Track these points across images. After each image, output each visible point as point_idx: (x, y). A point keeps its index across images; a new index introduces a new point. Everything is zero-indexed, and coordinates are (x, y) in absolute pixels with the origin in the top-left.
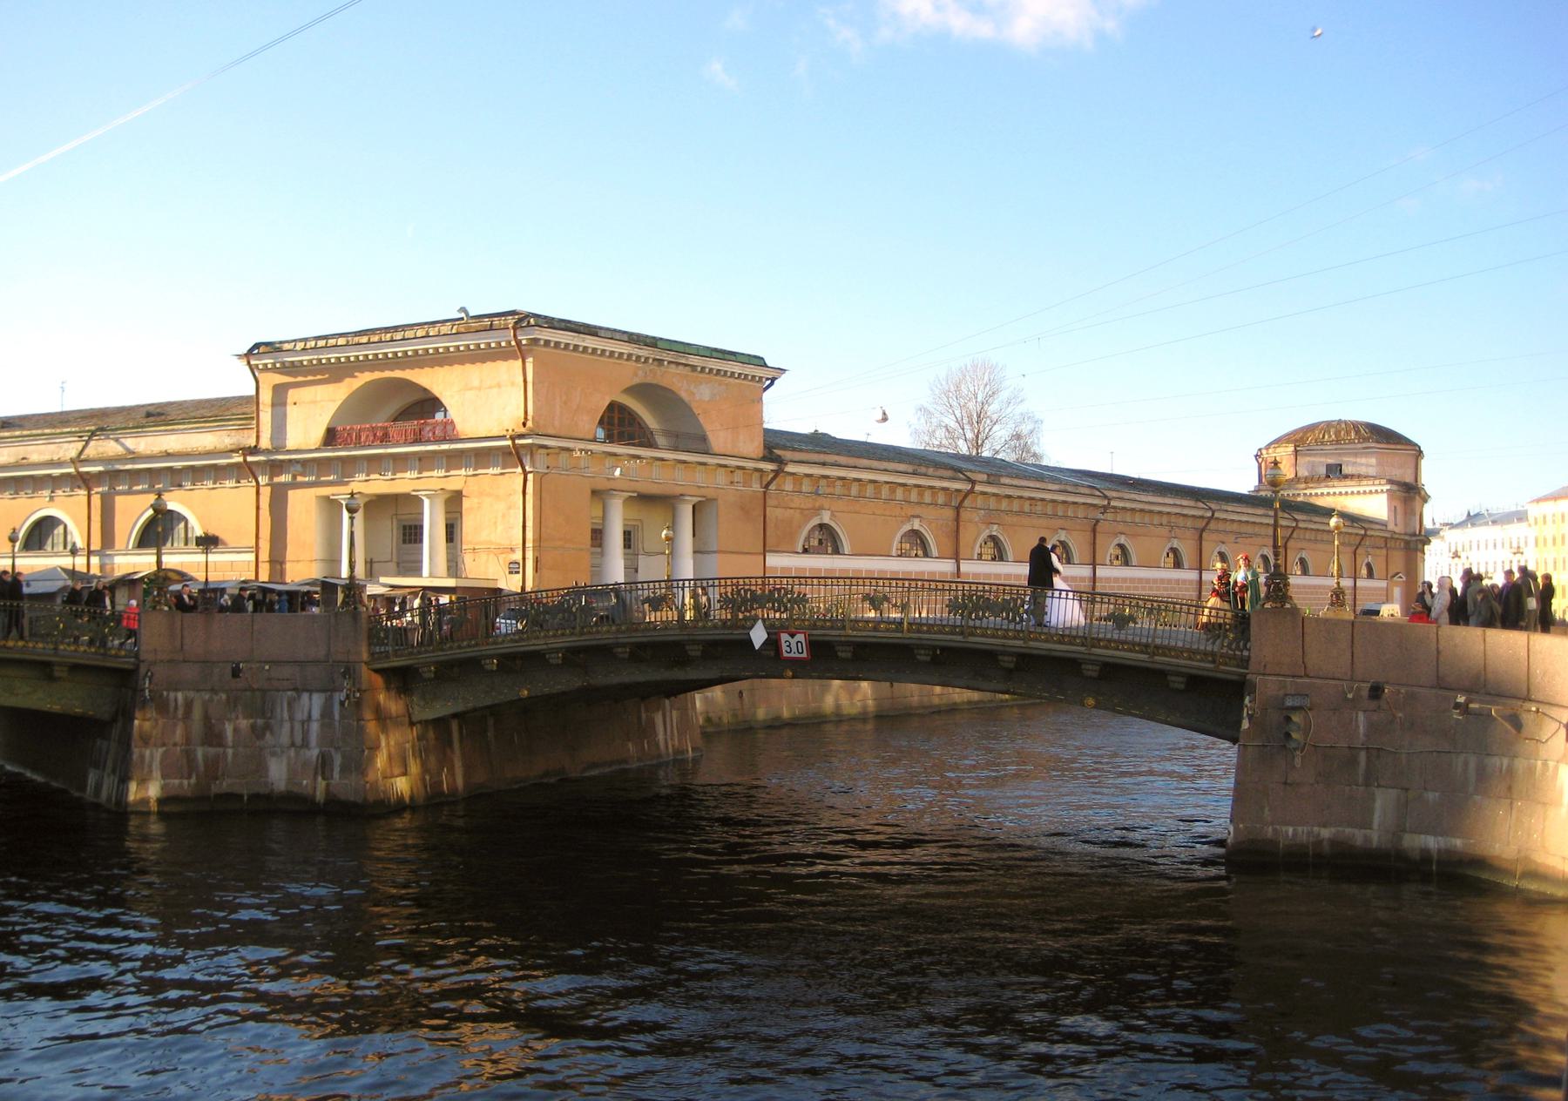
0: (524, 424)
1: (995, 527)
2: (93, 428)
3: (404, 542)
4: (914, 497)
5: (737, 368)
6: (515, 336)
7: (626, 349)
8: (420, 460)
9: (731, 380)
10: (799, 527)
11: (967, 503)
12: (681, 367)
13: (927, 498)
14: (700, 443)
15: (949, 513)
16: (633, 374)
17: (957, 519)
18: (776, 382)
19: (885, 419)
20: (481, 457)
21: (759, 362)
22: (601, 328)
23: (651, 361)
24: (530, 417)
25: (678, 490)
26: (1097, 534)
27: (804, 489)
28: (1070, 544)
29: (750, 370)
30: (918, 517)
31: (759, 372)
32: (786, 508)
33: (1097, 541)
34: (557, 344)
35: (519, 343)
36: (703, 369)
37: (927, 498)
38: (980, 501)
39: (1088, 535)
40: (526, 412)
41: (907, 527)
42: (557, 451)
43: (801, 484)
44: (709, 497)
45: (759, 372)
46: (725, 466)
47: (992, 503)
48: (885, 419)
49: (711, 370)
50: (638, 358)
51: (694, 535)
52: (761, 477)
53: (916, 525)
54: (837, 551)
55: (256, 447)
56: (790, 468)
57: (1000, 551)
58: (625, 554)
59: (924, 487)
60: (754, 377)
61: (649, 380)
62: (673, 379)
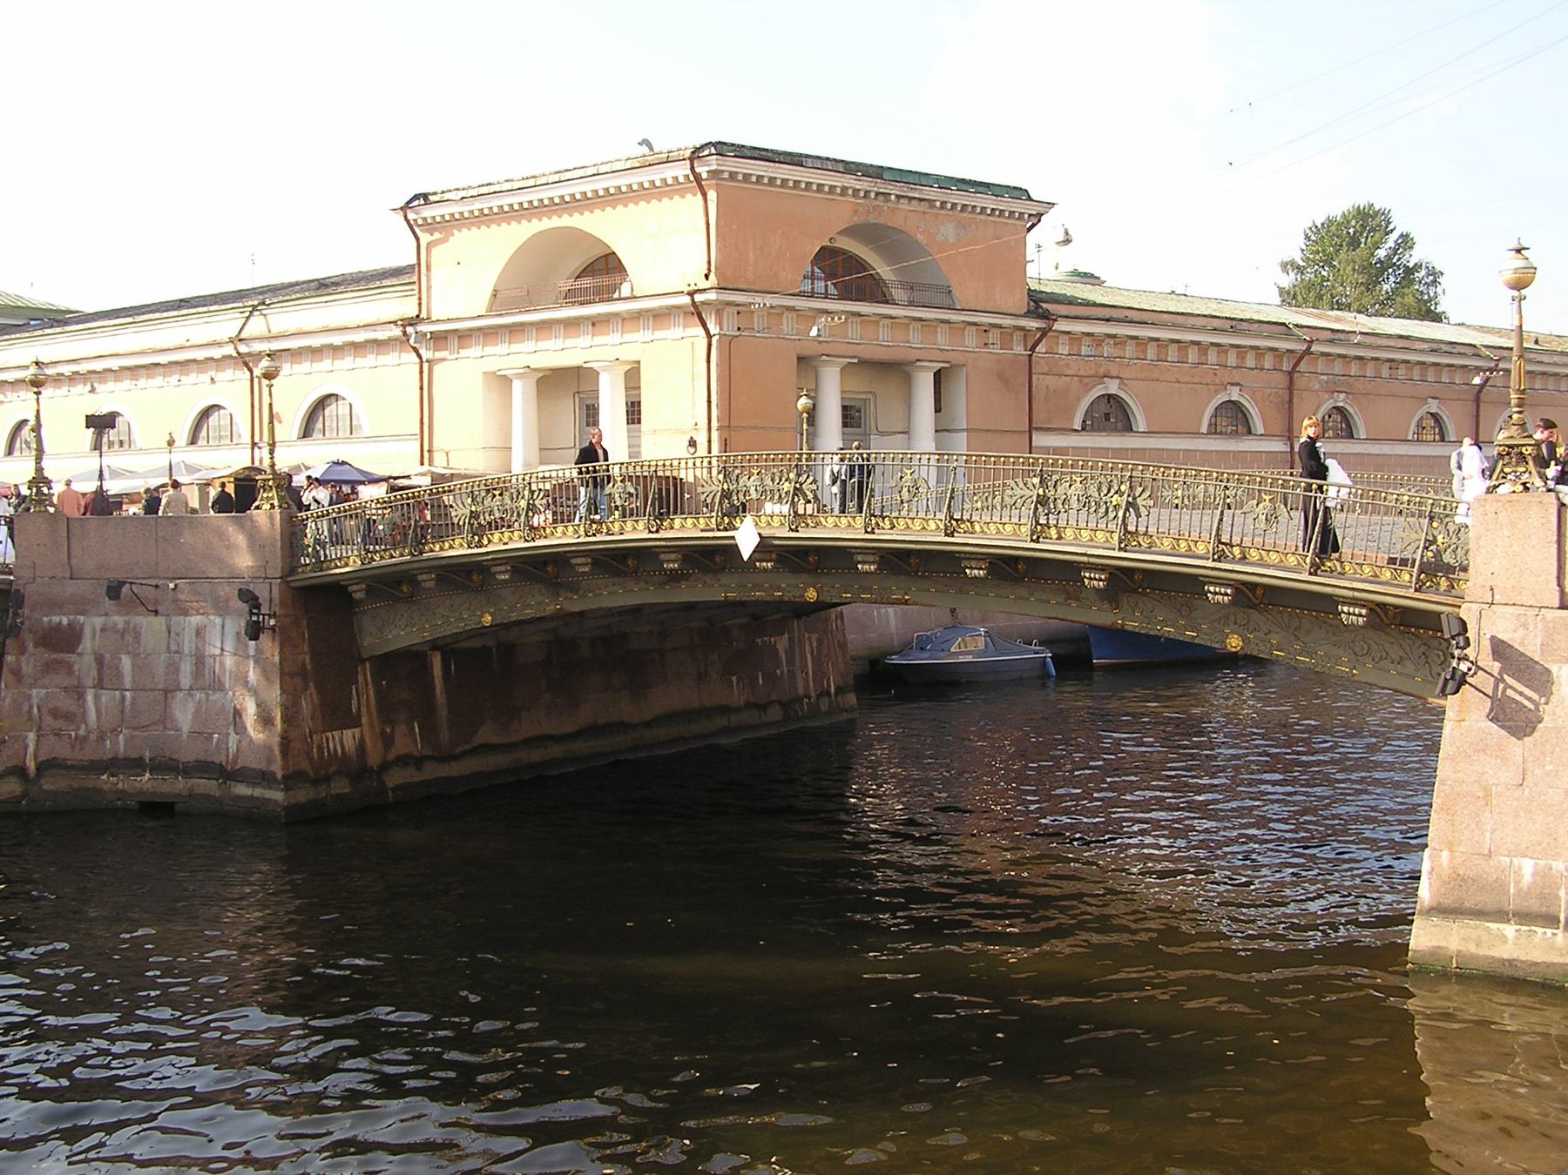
0: (707, 277)
1: (1342, 396)
2: (256, 303)
3: (588, 425)
4: (1232, 359)
5: (988, 202)
6: (692, 168)
7: (838, 181)
8: (593, 325)
9: (982, 217)
10: (1079, 399)
11: (1302, 367)
12: (914, 202)
13: (1250, 361)
14: (944, 297)
15: (1280, 380)
16: (843, 214)
17: (1291, 387)
18: (1043, 218)
19: (1067, 241)
20: (660, 317)
21: (1020, 193)
22: (807, 156)
23: (873, 195)
24: (713, 268)
25: (913, 355)
26: (1481, 404)
27: (1084, 350)
28: (1444, 417)
29: (1006, 204)
30: (1238, 384)
31: (1018, 206)
32: (1060, 375)
33: (1481, 413)
34: (747, 177)
35: (698, 177)
36: (943, 203)
37: (1250, 361)
38: (1321, 366)
39: (1471, 406)
40: (709, 263)
41: (1221, 398)
42: (962, 326)
43: (1206, 354)
44: (953, 362)
45: (1018, 206)
46: (975, 324)
47: (1338, 368)
48: (1067, 241)
49: (954, 205)
50: (856, 191)
51: (938, 410)
52: (1025, 336)
53: (1234, 394)
54: (1128, 427)
55: (418, 316)
56: (1061, 326)
57: (1349, 426)
58: (843, 434)
59: (1245, 347)
60: (1011, 213)
61: (872, 219)
62: (903, 217)
